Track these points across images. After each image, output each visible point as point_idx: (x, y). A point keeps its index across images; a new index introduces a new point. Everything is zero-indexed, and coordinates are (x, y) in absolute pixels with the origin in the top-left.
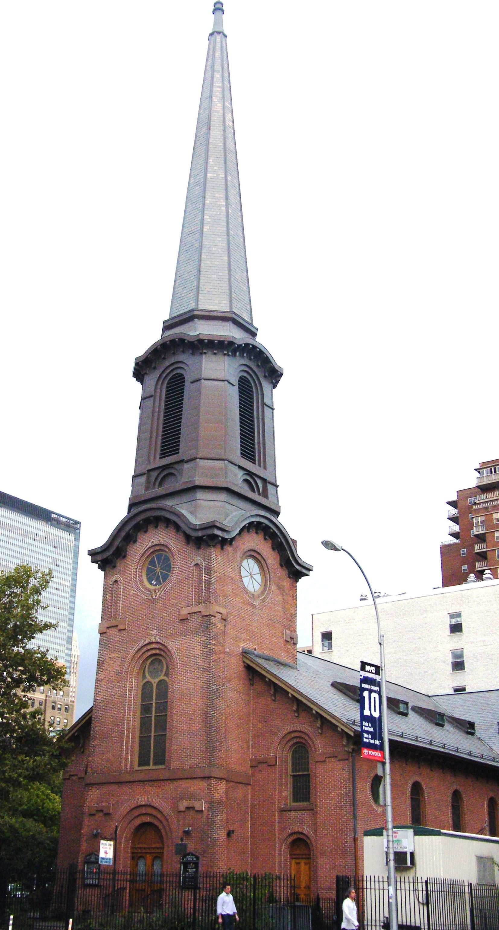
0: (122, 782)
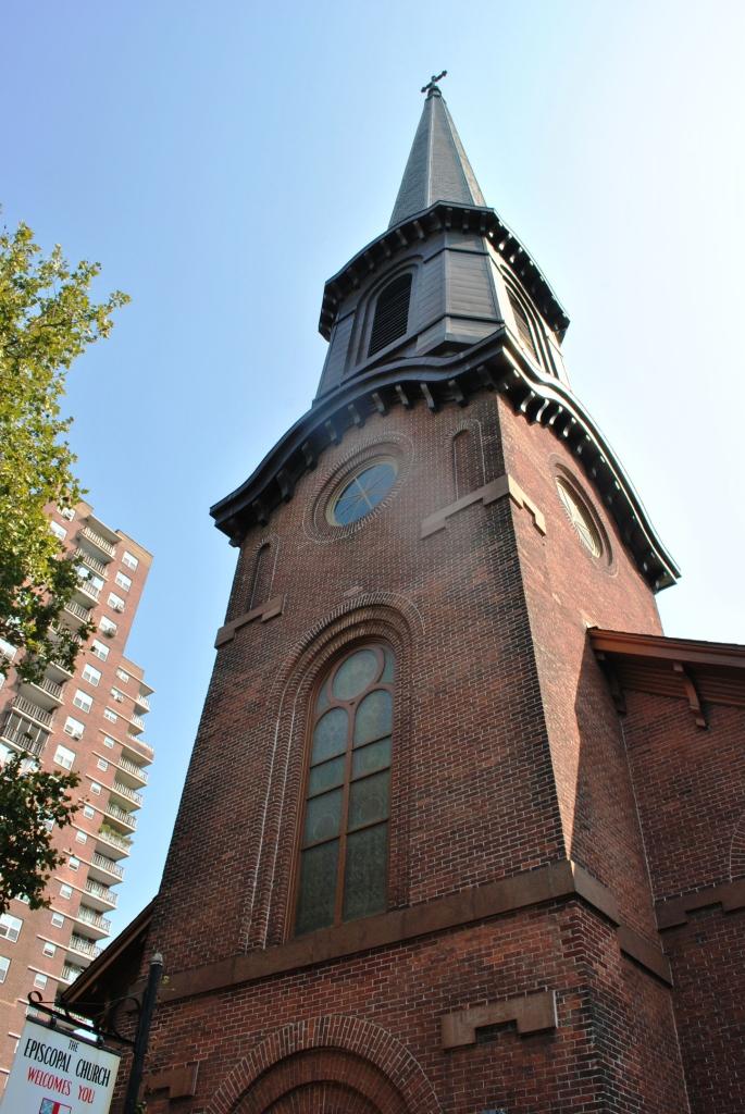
0: (243, 984)
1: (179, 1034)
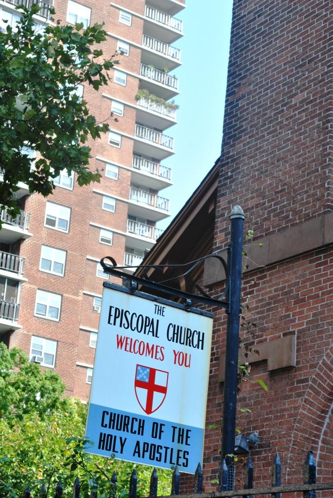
1: (269, 304)
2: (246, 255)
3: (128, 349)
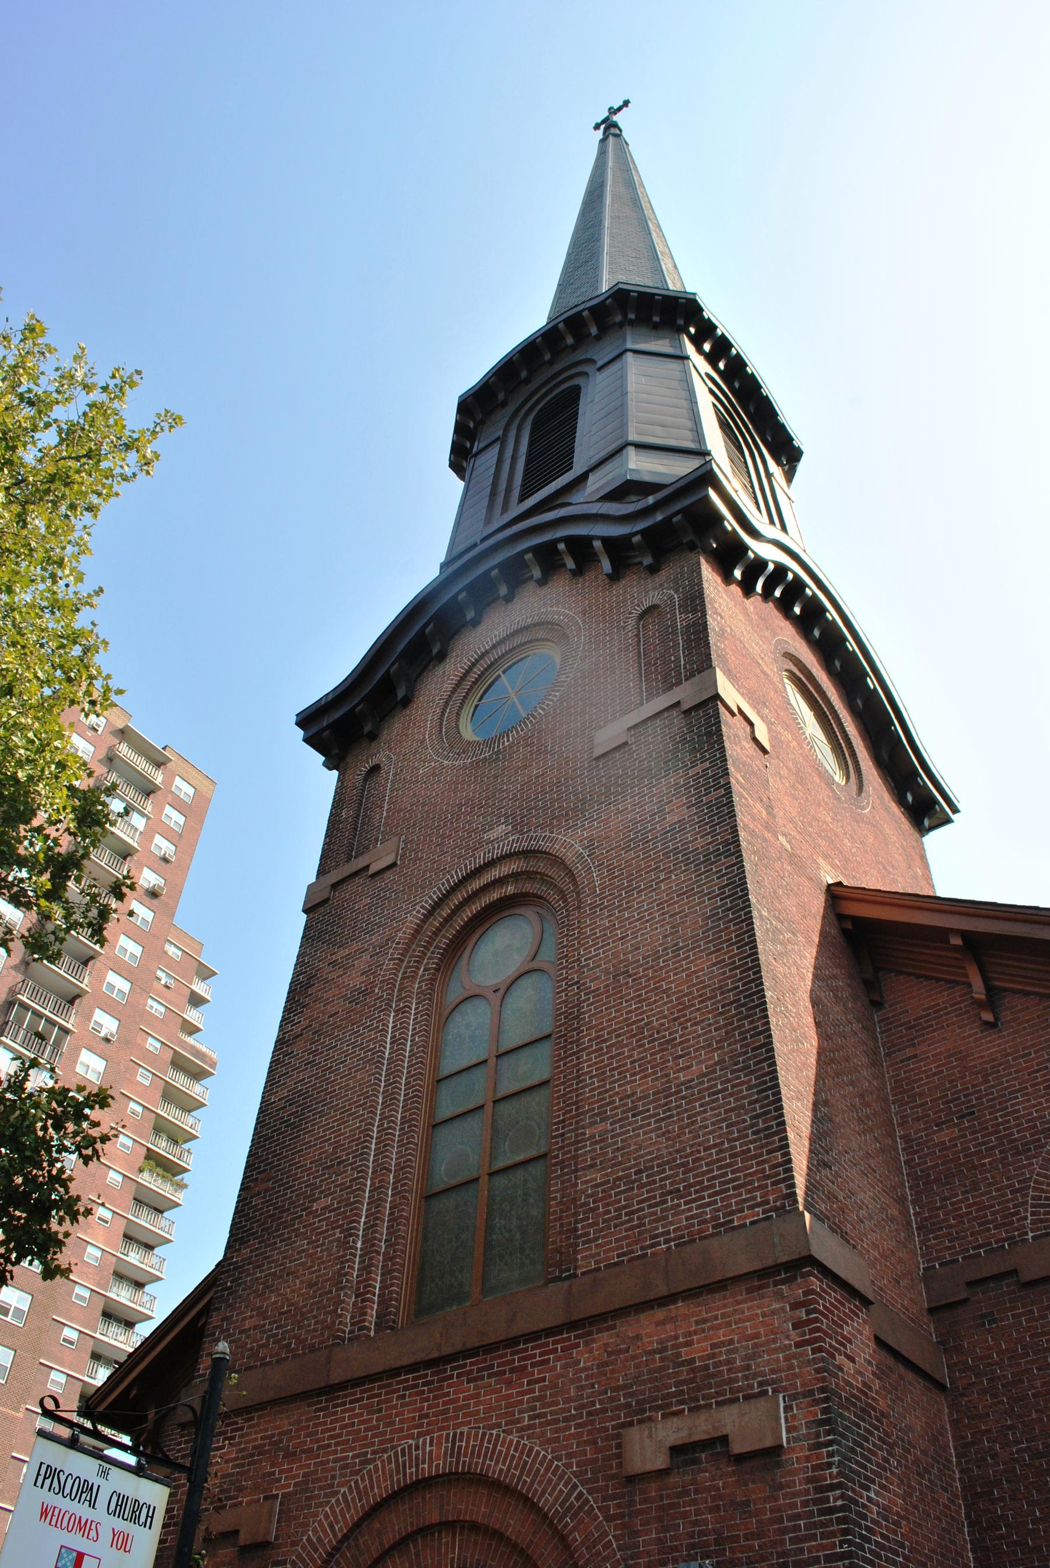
1: (252, 1455)
2: (224, 1405)
3: (53, 1523)
